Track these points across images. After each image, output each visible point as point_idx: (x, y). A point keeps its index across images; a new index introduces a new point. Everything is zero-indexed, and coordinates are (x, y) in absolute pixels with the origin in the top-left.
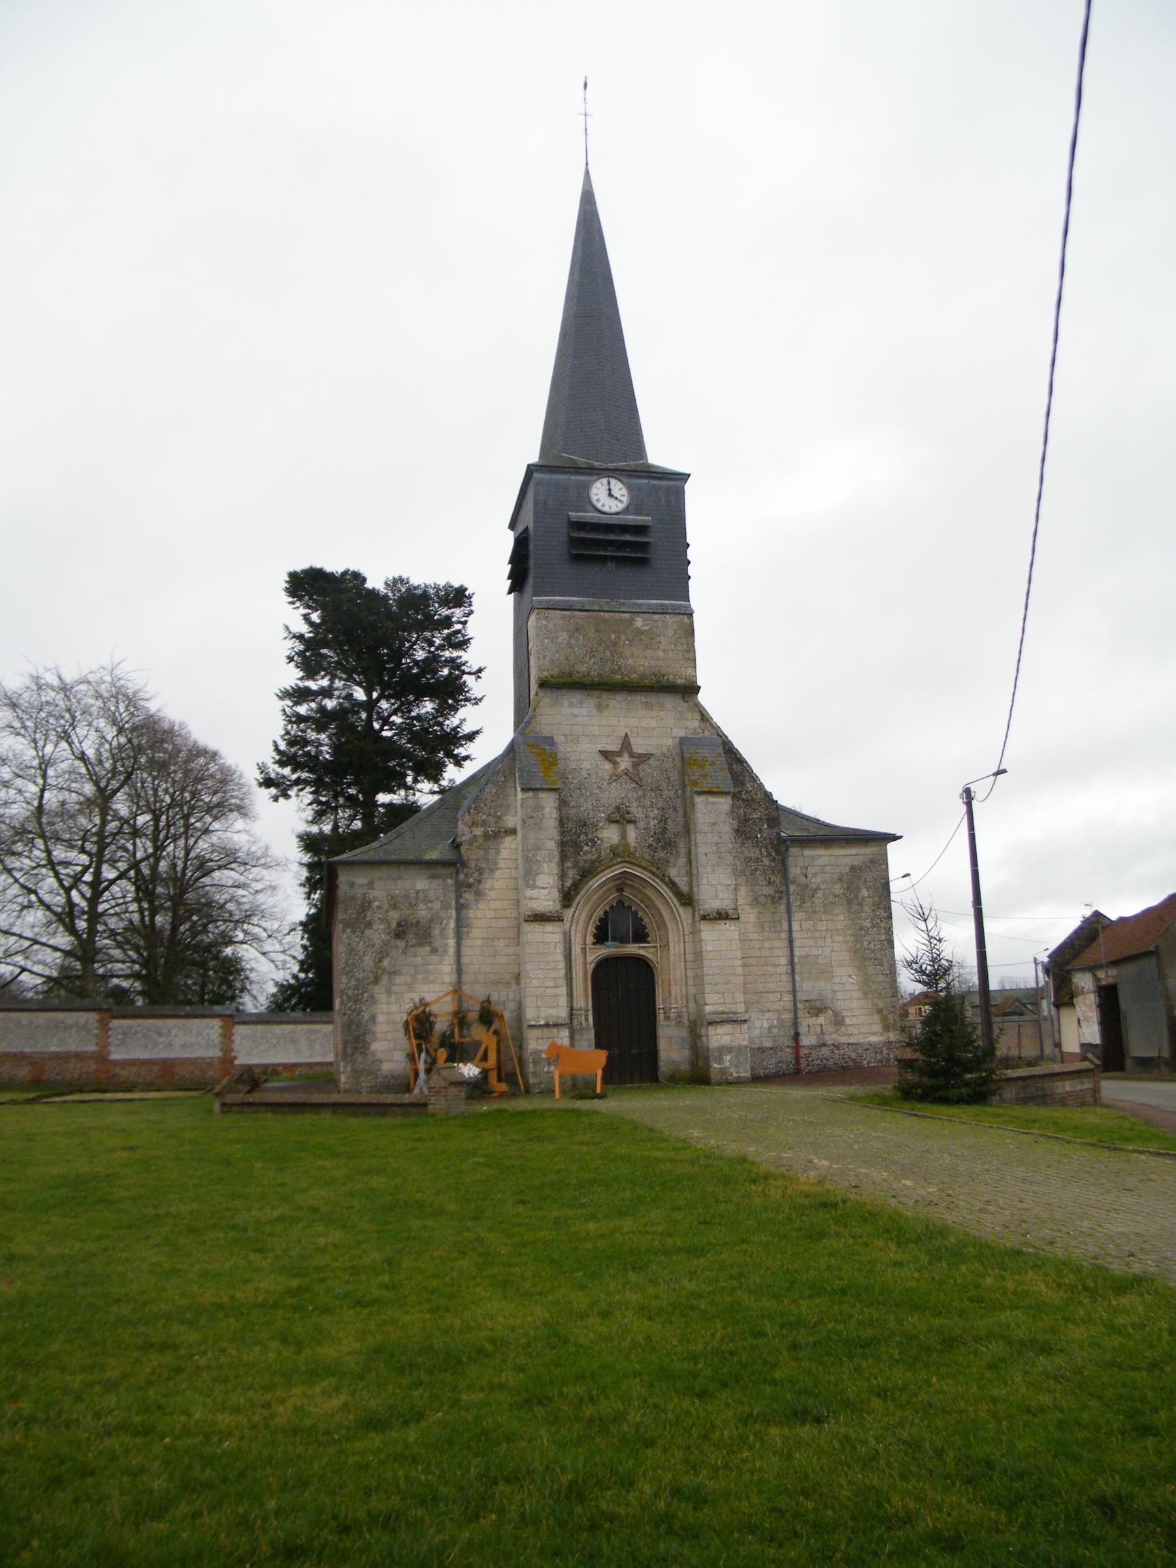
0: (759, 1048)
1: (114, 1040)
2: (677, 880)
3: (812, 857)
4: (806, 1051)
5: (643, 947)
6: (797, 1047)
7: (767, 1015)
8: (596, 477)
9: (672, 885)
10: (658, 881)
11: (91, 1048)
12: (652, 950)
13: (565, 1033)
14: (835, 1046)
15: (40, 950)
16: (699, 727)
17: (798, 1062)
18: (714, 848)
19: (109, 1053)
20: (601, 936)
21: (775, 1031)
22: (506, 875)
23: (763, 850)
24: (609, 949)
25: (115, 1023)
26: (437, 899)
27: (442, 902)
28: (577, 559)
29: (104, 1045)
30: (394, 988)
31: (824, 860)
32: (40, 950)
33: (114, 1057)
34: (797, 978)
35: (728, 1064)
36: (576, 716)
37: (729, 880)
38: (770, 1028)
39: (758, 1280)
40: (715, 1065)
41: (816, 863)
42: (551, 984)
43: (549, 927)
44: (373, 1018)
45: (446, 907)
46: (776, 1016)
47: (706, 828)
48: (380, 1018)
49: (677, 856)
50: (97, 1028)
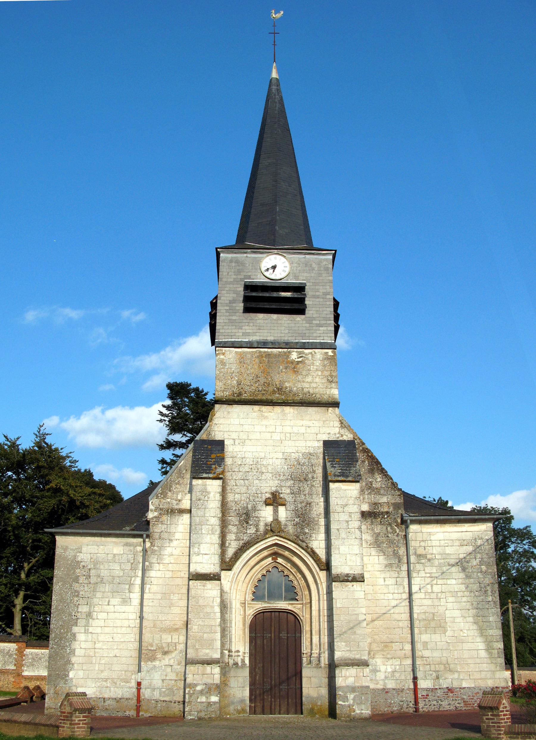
0: (384, 689)
1: (27, 661)
2: (317, 551)
3: (430, 534)
4: (424, 693)
5: (292, 604)
6: (415, 689)
7: (390, 662)
8: (265, 255)
9: (313, 554)
10: (303, 551)
11: (12, 667)
12: (300, 606)
13: (217, 670)
14: (449, 690)
15: (81, 621)
16: (339, 433)
17: (416, 702)
18: (345, 525)
19: (23, 671)
20: (257, 596)
21: (397, 675)
22: (182, 545)
23: (389, 528)
24: (260, 606)
25: (28, 651)
26: (129, 562)
27: (132, 564)
28: (247, 310)
29: (19, 664)
30: (91, 629)
31: (440, 536)
32: (81, 621)
33: (25, 673)
34: (416, 631)
35: (352, 702)
36: (243, 425)
37: (356, 549)
38: (394, 672)
39: (514, 571)
40: (340, 703)
41: (432, 538)
42: (208, 630)
43: (209, 584)
44: (73, 652)
45: (134, 569)
46: (399, 663)
47: (339, 509)
48: (78, 652)
49: (318, 533)
50: (16, 655)
